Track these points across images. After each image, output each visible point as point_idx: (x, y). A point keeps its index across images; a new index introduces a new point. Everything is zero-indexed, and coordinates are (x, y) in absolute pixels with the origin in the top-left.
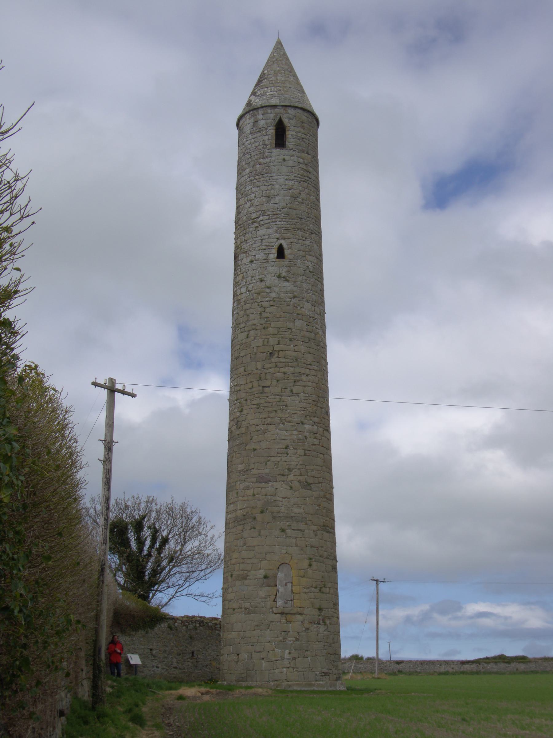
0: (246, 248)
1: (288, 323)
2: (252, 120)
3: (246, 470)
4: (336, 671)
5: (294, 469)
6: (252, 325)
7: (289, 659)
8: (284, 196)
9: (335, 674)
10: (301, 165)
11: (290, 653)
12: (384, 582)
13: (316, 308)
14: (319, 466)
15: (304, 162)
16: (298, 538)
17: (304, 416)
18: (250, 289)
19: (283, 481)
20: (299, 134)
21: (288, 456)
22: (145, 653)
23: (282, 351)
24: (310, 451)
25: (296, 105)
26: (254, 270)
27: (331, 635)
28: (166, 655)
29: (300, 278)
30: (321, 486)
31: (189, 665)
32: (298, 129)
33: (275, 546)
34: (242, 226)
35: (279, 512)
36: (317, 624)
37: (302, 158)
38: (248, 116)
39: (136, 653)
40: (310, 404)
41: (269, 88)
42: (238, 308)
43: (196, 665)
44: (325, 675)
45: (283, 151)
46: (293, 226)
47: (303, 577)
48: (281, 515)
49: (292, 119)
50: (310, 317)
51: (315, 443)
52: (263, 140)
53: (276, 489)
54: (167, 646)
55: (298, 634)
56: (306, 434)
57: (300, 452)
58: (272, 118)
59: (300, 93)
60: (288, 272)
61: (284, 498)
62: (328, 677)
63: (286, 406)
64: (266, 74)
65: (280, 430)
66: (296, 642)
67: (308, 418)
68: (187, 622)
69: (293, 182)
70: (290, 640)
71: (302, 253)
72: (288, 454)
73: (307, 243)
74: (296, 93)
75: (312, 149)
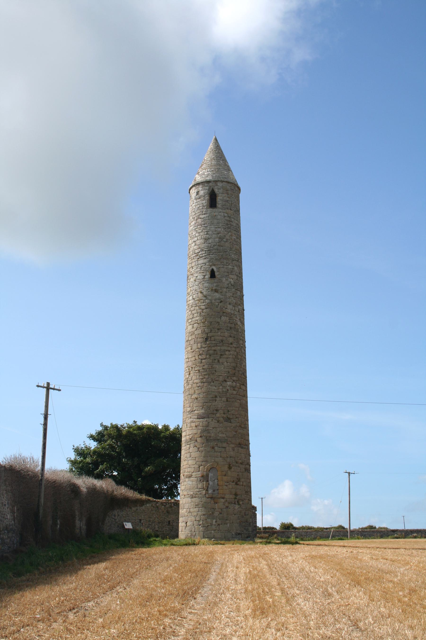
0: (192, 272)
1: (216, 319)
2: (196, 191)
3: (191, 411)
4: (247, 532)
5: (220, 410)
6: (195, 321)
7: (216, 525)
8: (215, 238)
9: (246, 534)
10: (226, 218)
11: (216, 522)
12: (354, 474)
13: (236, 308)
14: (237, 407)
15: (228, 215)
16: (222, 452)
17: (227, 377)
18: (194, 298)
19: (213, 418)
20: (225, 198)
21: (216, 402)
22: (136, 522)
23: (213, 336)
24: (230, 398)
25: (223, 180)
26: (197, 286)
27: (243, 510)
28: (151, 523)
29: (225, 290)
30: (238, 420)
31: (166, 529)
32: (224, 195)
33: (208, 457)
34: (190, 257)
35: (210, 437)
36: (233, 504)
37: (226, 213)
38: (194, 188)
39: (130, 522)
40: (231, 369)
41: (207, 170)
42: (188, 309)
43: (171, 529)
44: (238, 535)
45: (214, 210)
46: (220, 257)
47: (225, 475)
48: (212, 438)
49: (220, 189)
50: (232, 314)
51: (234, 393)
52: (202, 204)
53: (209, 422)
54: (151, 518)
55: (221, 510)
56: (229, 388)
57: (224, 399)
58: (207, 189)
59: (226, 171)
60: (217, 286)
61: (213, 428)
62: (241, 536)
63: (215, 371)
64: (206, 160)
65: (211, 386)
66: (220, 515)
67: (229, 378)
68: (165, 503)
69: (220, 229)
70: (216, 514)
71: (227, 274)
72: (216, 401)
73: (230, 267)
74: (223, 172)
75: (234, 207)
